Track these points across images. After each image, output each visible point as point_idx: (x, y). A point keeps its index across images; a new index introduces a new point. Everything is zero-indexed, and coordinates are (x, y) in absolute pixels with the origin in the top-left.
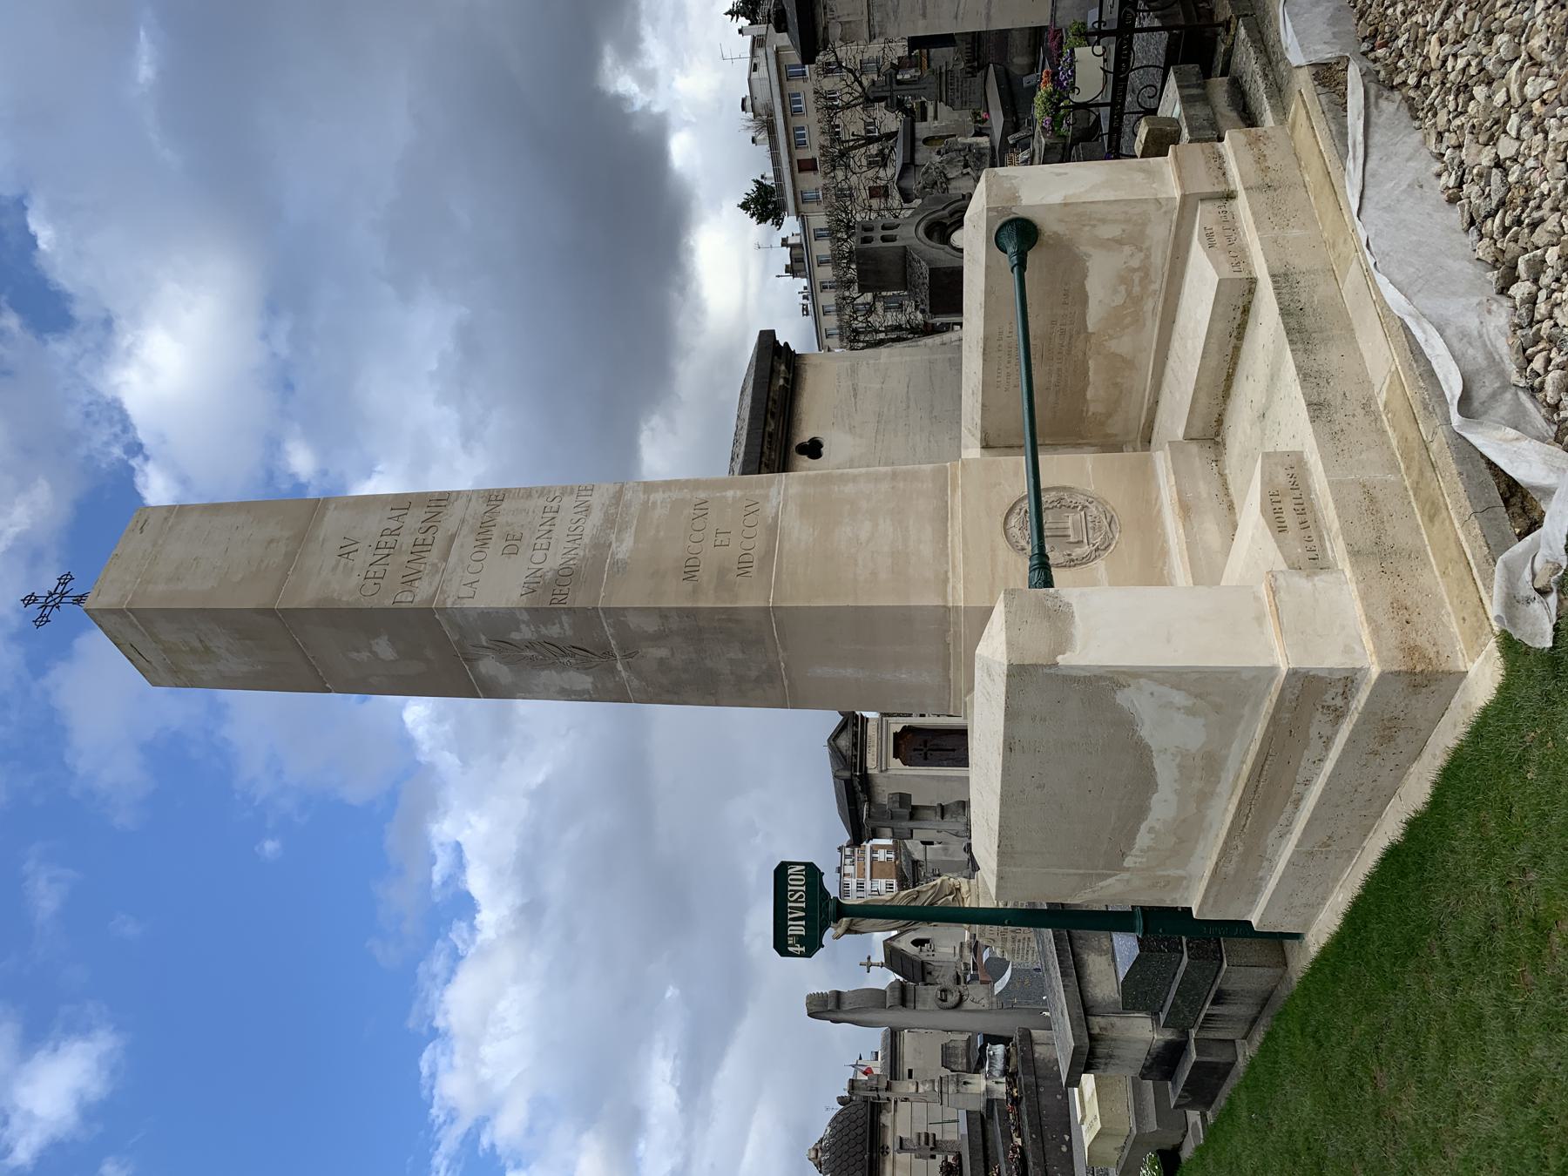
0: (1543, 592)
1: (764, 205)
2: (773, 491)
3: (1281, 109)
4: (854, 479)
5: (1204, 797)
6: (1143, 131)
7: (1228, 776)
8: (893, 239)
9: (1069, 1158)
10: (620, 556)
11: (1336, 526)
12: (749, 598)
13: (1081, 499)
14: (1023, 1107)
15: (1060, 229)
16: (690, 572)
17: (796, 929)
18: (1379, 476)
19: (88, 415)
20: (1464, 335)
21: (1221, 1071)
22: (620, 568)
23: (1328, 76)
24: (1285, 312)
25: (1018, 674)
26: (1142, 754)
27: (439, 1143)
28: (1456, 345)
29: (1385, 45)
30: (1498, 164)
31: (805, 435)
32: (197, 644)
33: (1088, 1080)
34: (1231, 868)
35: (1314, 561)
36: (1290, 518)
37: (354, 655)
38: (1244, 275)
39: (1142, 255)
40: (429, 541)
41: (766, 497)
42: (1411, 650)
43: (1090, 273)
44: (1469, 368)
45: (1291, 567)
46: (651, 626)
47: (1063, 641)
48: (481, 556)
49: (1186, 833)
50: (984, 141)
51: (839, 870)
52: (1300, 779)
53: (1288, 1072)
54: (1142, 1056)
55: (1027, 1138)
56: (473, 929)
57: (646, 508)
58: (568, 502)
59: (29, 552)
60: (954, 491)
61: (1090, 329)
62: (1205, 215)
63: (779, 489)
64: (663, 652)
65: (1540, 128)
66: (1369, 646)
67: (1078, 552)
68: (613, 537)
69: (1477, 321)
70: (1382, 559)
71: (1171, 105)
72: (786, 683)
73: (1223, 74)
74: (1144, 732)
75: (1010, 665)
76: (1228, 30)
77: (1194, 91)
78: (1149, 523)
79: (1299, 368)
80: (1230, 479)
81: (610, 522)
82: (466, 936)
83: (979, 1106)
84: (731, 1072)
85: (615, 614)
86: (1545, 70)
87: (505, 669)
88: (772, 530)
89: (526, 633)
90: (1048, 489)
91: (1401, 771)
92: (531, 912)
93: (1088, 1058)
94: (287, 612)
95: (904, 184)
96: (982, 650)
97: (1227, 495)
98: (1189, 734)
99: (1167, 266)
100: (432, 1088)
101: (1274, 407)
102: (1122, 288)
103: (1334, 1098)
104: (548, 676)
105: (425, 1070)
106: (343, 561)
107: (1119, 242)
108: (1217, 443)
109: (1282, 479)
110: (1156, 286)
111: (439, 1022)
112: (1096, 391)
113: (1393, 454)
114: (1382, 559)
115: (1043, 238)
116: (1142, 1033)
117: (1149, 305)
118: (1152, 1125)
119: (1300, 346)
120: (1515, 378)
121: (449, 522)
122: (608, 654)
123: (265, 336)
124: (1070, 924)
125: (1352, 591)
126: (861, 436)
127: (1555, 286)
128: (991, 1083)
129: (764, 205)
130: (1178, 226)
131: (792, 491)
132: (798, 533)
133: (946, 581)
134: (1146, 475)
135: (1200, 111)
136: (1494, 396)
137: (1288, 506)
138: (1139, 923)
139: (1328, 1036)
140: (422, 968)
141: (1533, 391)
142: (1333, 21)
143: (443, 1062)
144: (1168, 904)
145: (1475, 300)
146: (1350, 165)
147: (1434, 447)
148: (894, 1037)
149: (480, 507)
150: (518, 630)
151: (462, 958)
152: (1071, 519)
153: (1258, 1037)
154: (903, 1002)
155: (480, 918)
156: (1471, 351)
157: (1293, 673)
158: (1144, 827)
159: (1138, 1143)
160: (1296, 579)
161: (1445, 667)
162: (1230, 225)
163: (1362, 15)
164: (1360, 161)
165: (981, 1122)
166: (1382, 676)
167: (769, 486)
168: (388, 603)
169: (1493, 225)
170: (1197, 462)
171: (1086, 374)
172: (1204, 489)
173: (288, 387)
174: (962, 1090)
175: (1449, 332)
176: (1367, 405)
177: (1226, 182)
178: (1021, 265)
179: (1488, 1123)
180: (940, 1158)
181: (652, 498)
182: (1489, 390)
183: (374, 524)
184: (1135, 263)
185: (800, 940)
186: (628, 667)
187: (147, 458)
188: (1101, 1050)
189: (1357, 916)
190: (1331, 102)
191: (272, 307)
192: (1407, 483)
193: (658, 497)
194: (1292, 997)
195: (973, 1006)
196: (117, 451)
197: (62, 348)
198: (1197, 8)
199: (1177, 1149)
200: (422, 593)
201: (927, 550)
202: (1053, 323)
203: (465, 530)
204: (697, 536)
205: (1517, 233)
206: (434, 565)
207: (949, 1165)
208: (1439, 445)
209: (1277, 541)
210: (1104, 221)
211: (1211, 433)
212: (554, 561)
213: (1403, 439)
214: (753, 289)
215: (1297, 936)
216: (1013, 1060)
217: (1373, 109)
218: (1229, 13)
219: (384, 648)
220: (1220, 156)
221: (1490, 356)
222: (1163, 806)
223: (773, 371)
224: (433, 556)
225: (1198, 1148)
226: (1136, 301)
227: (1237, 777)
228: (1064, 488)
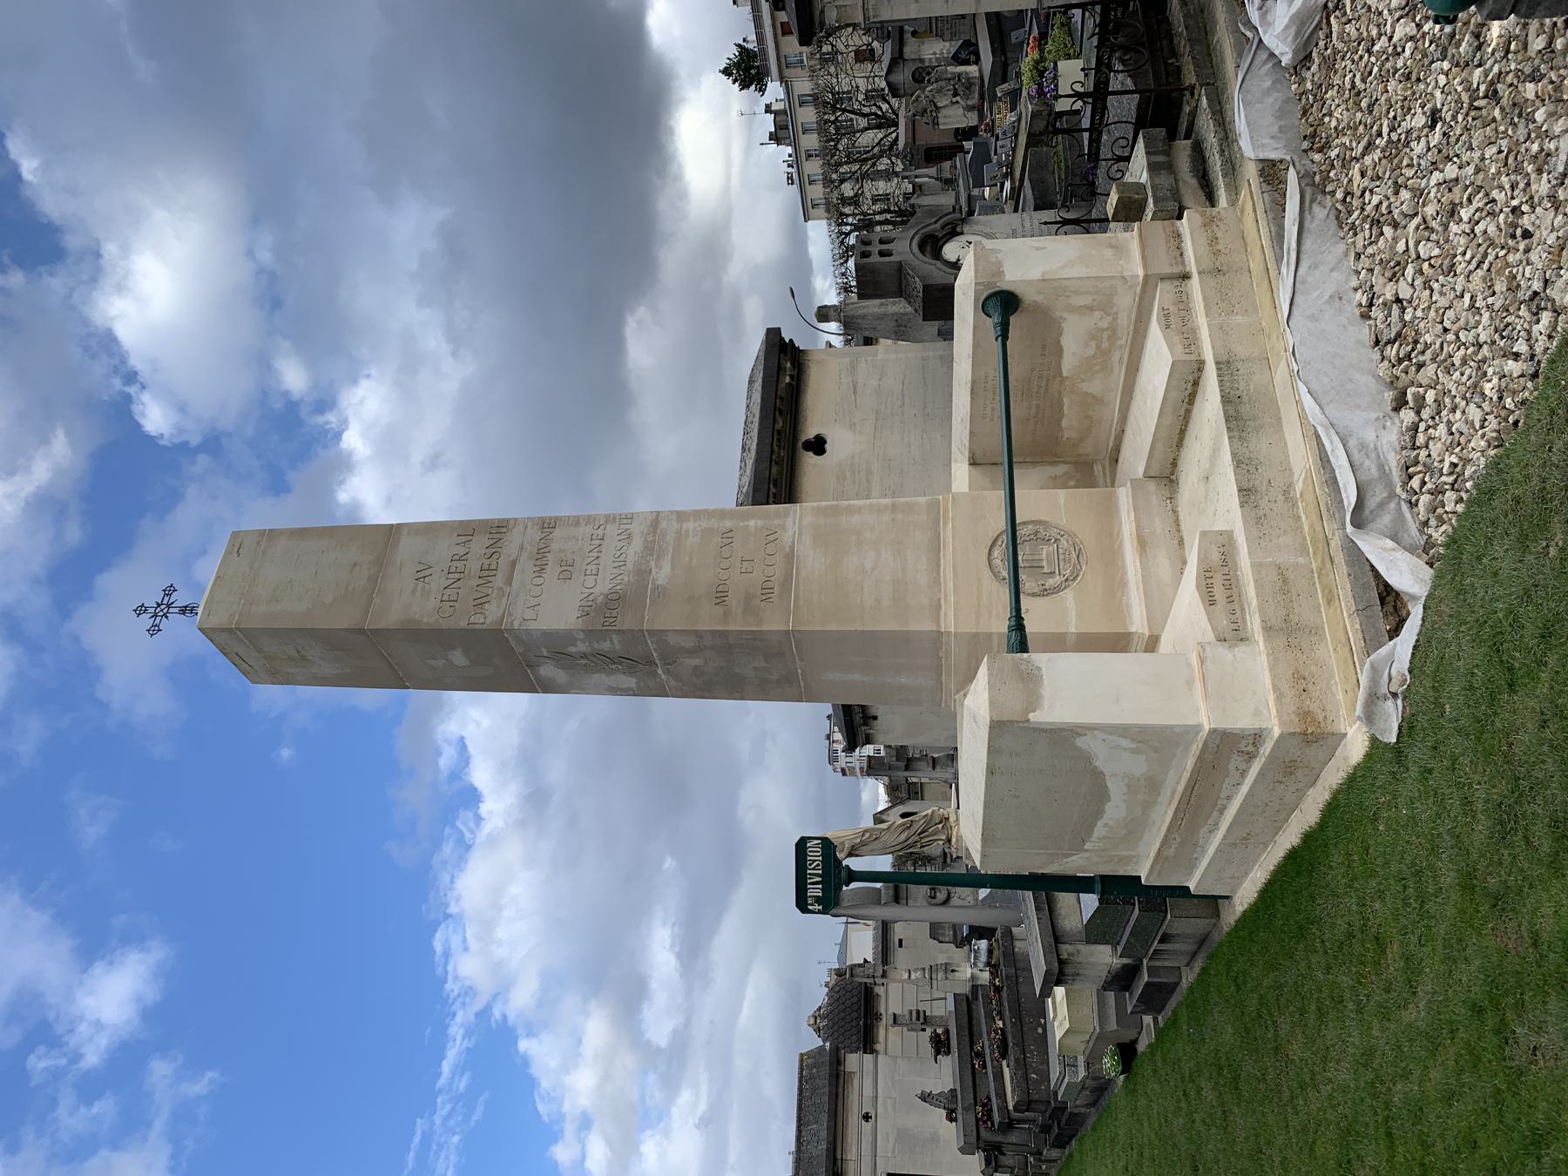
0: (1395, 695)
1: (747, 70)
2: (790, 520)
3: (1233, 189)
4: (859, 510)
5: (1148, 806)
6: (1114, 198)
7: (1166, 792)
8: (889, 254)
9: (1043, 1040)
10: (660, 582)
11: (1254, 603)
12: (773, 624)
13: (1054, 532)
14: (1004, 994)
15: (1039, 298)
16: (721, 597)
17: (815, 891)
18: (1292, 559)
19: (86, 349)
20: (1363, 446)
21: (1171, 988)
22: (661, 593)
23: (1271, 173)
24: (1226, 400)
25: (998, 728)
26: (1098, 778)
27: (454, 1015)
28: (1356, 457)
29: (1320, 150)
30: (1398, 300)
31: (810, 432)
33: (1059, 991)
34: (1171, 852)
35: (1234, 635)
36: (1219, 593)
37: (432, 662)
38: (1193, 357)
41: (783, 527)
42: (1305, 715)
43: (1065, 332)
44: (1363, 477)
46: (688, 643)
47: (1033, 702)
48: (540, 581)
49: (1133, 829)
50: (972, 70)
51: (828, 737)
52: (1223, 795)
53: (1217, 1004)
54: (1104, 974)
56: (479, 819)
57: (680, 536)
58: (612, 530)
59: (44, 505)
60: (945, 523)
61: (1065, 374)
62: (1163, 295)
63: (791, 520)
64: (697, 662)
65: (1427, 285)
66: (1274, 711)
67: (1050, 582)
70: (1289, 636)
71: (1138, 170)
73: (1187, 137)
74: (1099, 764)
75: (992, 721)
76: (1192, 94)
77: (1161, 158)
78: (1111, 556)
79: (1234, 455)
80: (1181, 516)
81: (651, 549)
82: (472, 824)
83: (965, 989)
84: (728, 936)
85: (659, 635)
86: (1434, 237)
87: (562, 672)
88: (790, 557)
89: (582, 647)
90: (1024, 523)
91: (1301, 794)
92: (536, 800)
93: (1060, 974)
94: (376, 632)
95: (893, 78)
96: (968, 701)
97: (1179, 531)
98: (1139, 766)
100: (446, 965)
101: (1212, 495)
103: (1247, 1031)
104: (596, 678)
105: (438, 946)
106: (420, 584)
107: (1091, 309)
108: (1172, 481)
109: (1215, 557)
110: (1122, 342)
111: (453, 909)
112: (1070, 422)
114: (1289, 636)
115: (1024, 305)
116: (1104, 958)
117: (1116, 356)
118: (1112, 1025)
120: (1399, 490)
121: (510, 547)
122: (651, 663)
123: (250, 253)
124: (1046, 886)
125: (1263, 660)
126: (861, 433)
127: (1431, 423)
128: (976, 971)
129: (747, 70)
130: (1141, 299)
131: (805, 522)
132: (812, 561)
133: (939, 607)
134: (1109, 511)
135: (1165, 180)
136: (1381, 505)
137: (1218, 581)
138: (1098, 886)
139: (1245, 983)
140: (436, 860)
141: (1413, 505)
142: (1281, 113)
143: (455, 942)
144: (1121, 873)
145: (1374, 415)
146: (1284, 270)
147: (1333, 544)
148: (885, 929)
149: (534, 534)
151: (469, 847)
152: (1045, 551)
153: (1198, 965)
154: (897, 899)
155: (485, 808)
156: (1367, 463)
157: (1213, 731)
158: (1100, 823)
159: (1101, 1038)
161: (1330, 729)
162: (1184, 303)
163: (1305, 113)
164: (1293, 267)
165: (967, 1004)
166: (1282, 736)
167: (787, 516)
168: (463, 624)
169: (1391, 352)
170: (1154, 499)
171: (1061, 409)
172: (1159, 525)
173: (276, 304)
174: (951, 976)
175: (1352, 443)
176: (1287, 492)
177: (1183, 262)
178: (1004, 335)
179: (1344, 1075)
180: (929, 1031)
182: (1378, 499)
183: (444, 550)
184: (1104, 324)
185: (818, 900)
186: (667, 672)
187: (143, 387)
188: (1069, 970)
189: (1269, 893)
190: (1273, 201)
191: (255, 219)
192: (1314, 565)
193: (690, 525)
194: (1221, 945)
195: (960, 903)
196: (117, 383)
197: (55, 283)
198: (1166, 65)
199: (1135, 1041)
200: (492, 614)
202: (1033, 369)
203: (525, 555)
204: (726, 564)
205: (1407, 367)
207: (938, 1036)
208: (1335, 543)
209: (1208, 613)
210: (1076, 293)
211: (1167, 475)
212: (602, 587)
213: (1312, 527)
214: (735, 170)
215: (1227, 897)
216: (996, 953)
217: (1307, 216)
218: (1194, 80)
219: (458, 657)
220: (1179, 236)
221: (1381, 467)
222: (1115, 810)
223: (780, 369)
224: (499, 580)
225: (1150, 1045)
226: (1104, 354)
227: (1174, 792)
228: (1040, 522)
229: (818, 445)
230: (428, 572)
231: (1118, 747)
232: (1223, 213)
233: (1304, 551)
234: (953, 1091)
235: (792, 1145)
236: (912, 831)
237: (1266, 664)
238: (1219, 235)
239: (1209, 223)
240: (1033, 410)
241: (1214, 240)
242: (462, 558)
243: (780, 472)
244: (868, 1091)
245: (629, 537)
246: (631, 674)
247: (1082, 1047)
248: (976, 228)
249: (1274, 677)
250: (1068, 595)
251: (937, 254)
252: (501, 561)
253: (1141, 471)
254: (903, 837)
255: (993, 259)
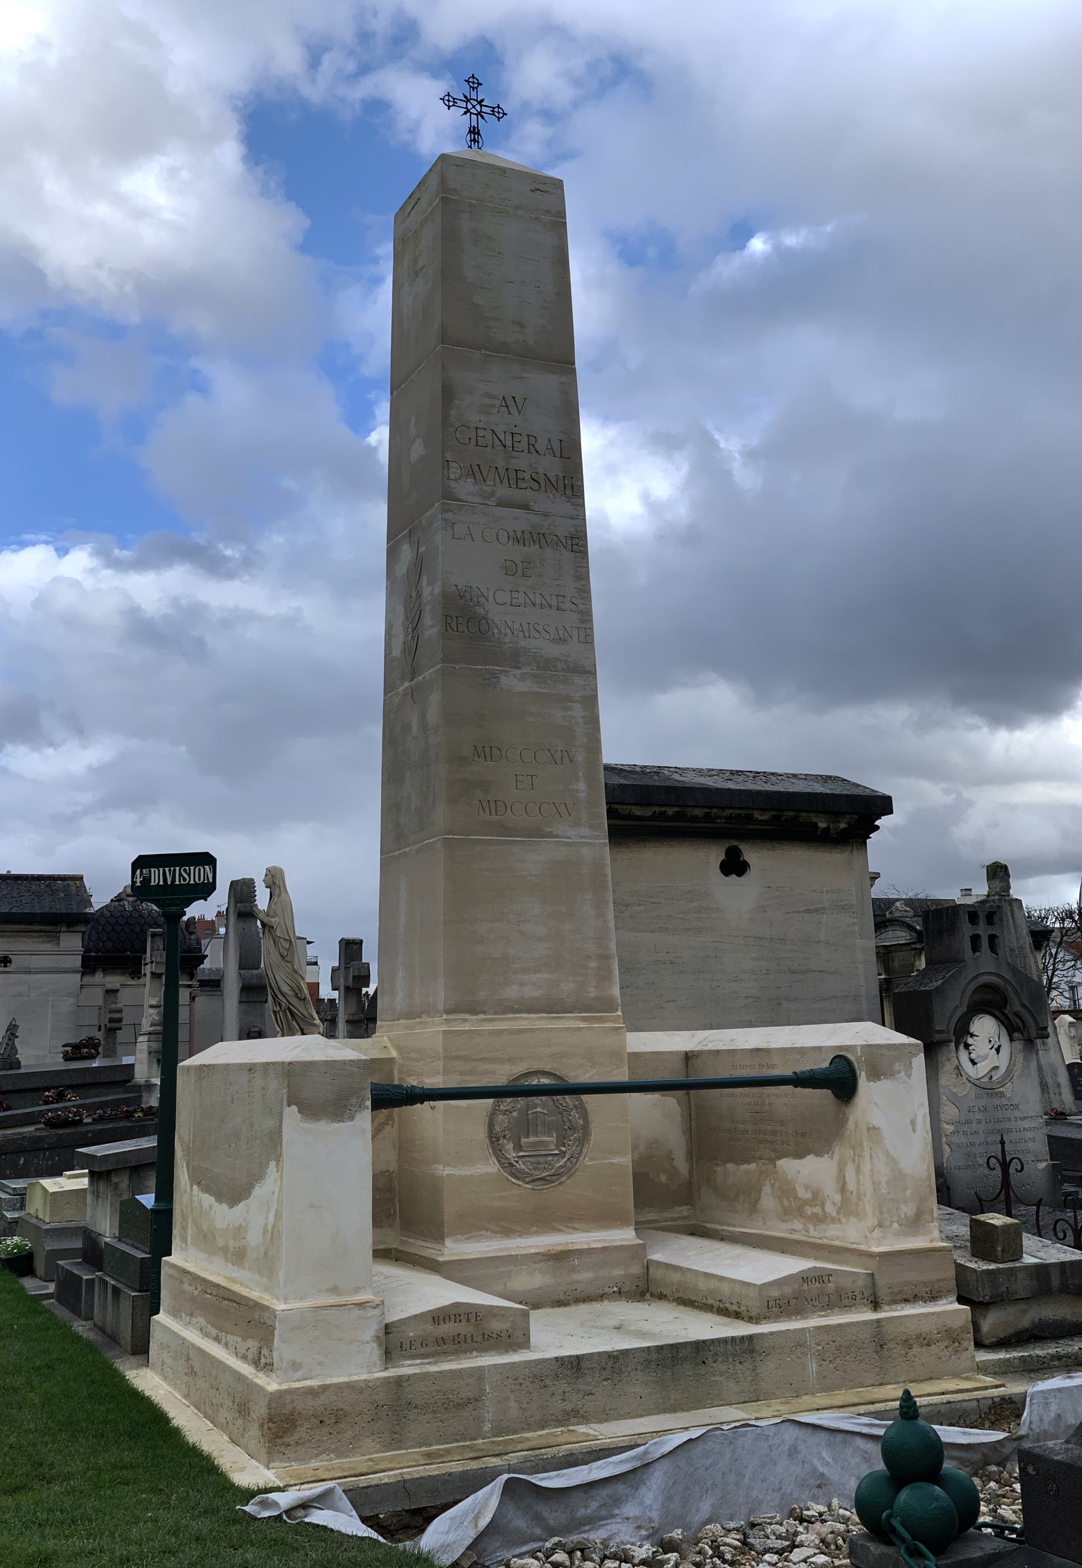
2: (586, 831)
10: (504, 680)
11: (433, 1369)
15: (850, 1125)
17: (156, 877)
20: (617, 1501)
23: (1005, 1411)
24: (699, 1347)
28: (605, 1492)
31: (751, 855)
32: (420, 264)
35: (393, 1341)
36: (448, 1329)
37: (413, 421)
39: (834, 1214)
40: (521, 484)
45: (387, 1326)
48: (503, 537)
49: (207, 1240)
55: (89, 1128)
60: (585, 1019)
61: (779, 1163)
63: (587, 836)
68: (527, 670)
69: (631, 1515)
72: (397, 853)
79: (626, 1352)
81: (546, 665)
87: (404, 570)
88: (537, 833)
97: (577, 1301)
98: (254, 1238)
99: (825, 1241)
102: (809, 1196)
104: (400, 609)
107: (843, 1189)
109: (496, 1326)
112: (734, 1172)
113: (515, 1433)
117: (798, 1225)
118: (50, 1245)
119: (655, 1356)
121: (543, 501)
131: (586, 852)
132: (532, 860)
133: (474, 1012)
135: (1022, 1286)
138: (163, 1206)
147: (494, 1460)
150: (428, 584)
156: (594, 1505)
158: (212, 1199)
160: (375, 1327)
175: (621, 1488)
181: (577, 705)
182: (546, 1514)
184: (830, 1209)
185: (146, 881)
193: (578, 711)
201: (511, 992)
202: (782, 1123)
206: (493, 494)
210: (858, 1170)
213: (527, 1439)
224: (504, 491)
229: (734, 866)
230: (513, 410)
231: (269, 1211)
232: (967, 1354)
233: (498, 1431)
234: (18, 1065)
235: (15, 871)
236: (294, 1000)
237: (355, 1378)
238: (933, 1347)
239: (951, 1336)
240: (741, 1126)
241: (926, 1342)
242: (532, 449)
243: (696, 819)
244: (37, 962)
245: (562, 641)
246: (404, 651)
247: (32, 1212)
248: (1020, 1058)
249: (339, 1387)
250: (491, 1167)
251: (978, 1008)
252: (529, 492)
253: (657, 1257)
254: (285, 989)
255: (897, 1066)
